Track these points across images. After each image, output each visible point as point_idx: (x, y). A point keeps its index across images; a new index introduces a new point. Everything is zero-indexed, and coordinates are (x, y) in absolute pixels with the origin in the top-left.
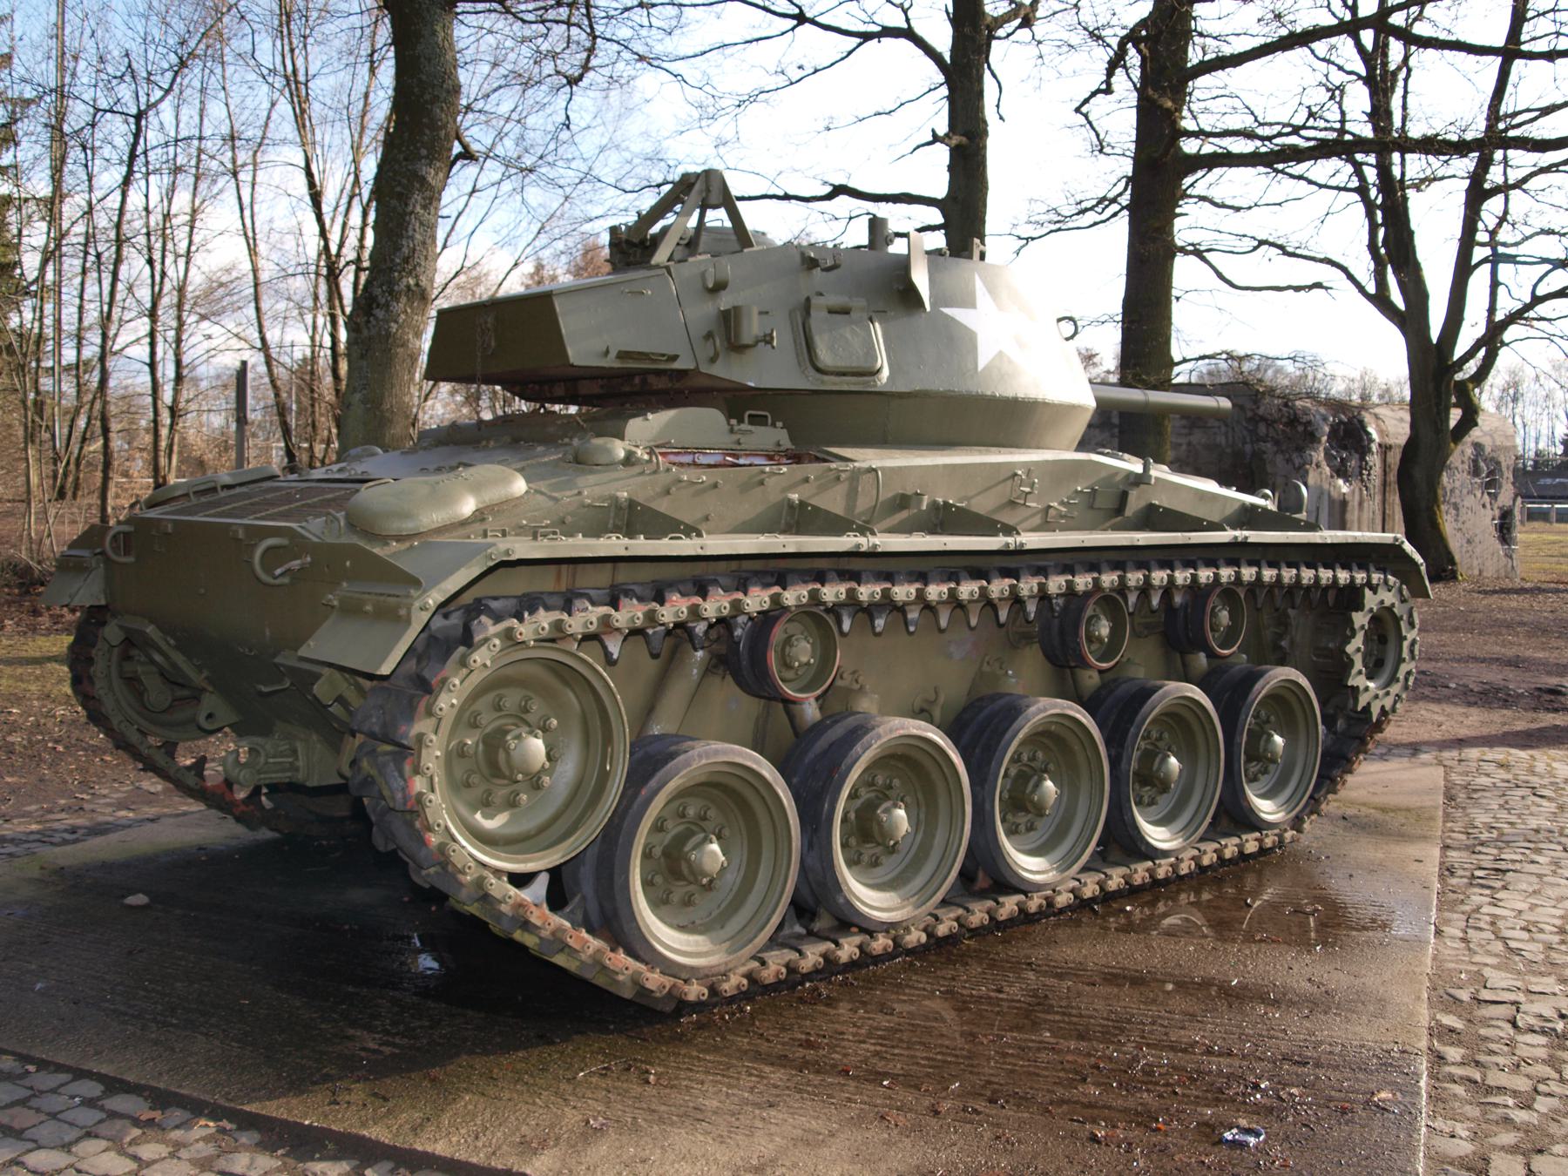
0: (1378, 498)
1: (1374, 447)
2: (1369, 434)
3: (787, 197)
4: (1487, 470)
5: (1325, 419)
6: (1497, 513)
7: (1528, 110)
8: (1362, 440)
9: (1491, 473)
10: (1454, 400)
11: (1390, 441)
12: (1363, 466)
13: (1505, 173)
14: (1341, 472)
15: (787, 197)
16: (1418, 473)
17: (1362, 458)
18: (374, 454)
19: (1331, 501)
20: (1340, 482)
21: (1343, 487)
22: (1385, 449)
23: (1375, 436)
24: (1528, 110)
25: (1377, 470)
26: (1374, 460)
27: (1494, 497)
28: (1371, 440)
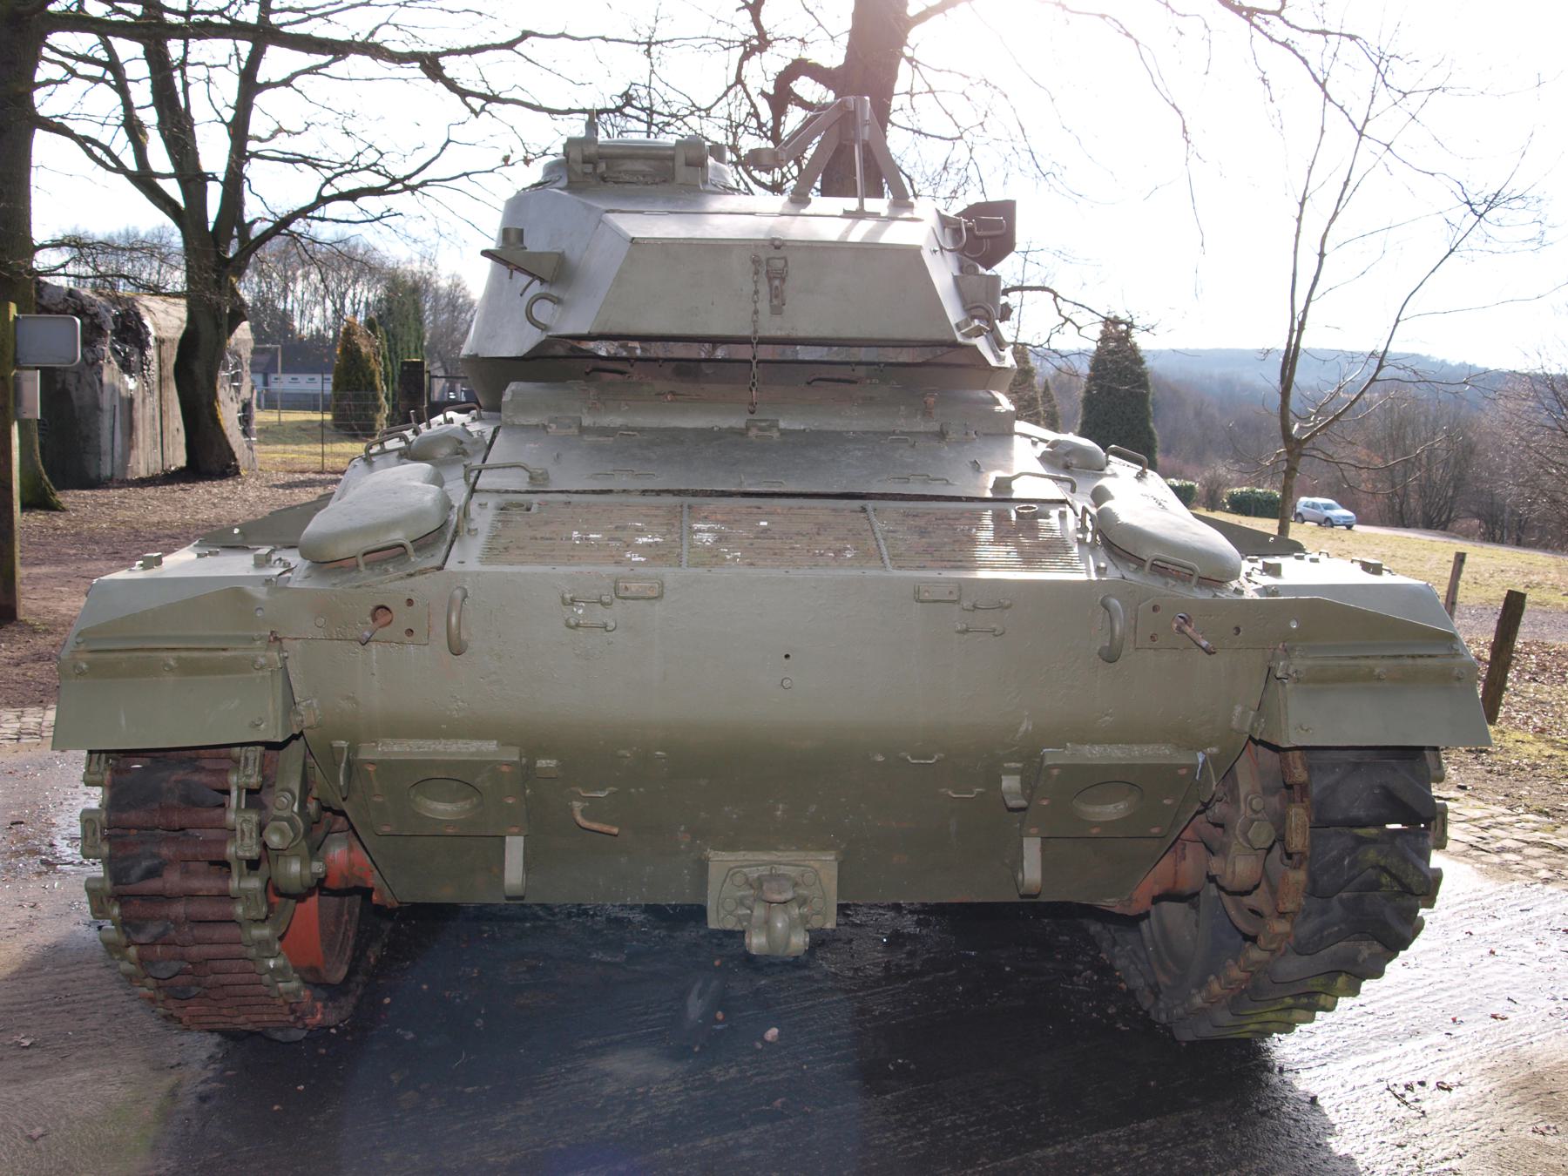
0: (157, 393)
1: (151, 341)
2: (145, 327)
3: (1322, 255)
4: (284, 349)
5: (108, 311)
6: (240, 406)
7: (291, 9)
8: (139, 333)
9: (235, 366)
10: (818, 185)
11: (163, 335)
12: (144, 362)
13: (186, 52)
14: (126, 367)
15: (1322, 255)
16: (199, 368)
17: (142, 353)
18: (77, 244)
19: (122, 399)
20: (126, 377)
21: (132, 384)
22: (160, 342)
23: (151, 329)
24: (291, 9)
25: (154, 366)
26: (151, 353)
27: (238, 389)
28: (148, 334)
